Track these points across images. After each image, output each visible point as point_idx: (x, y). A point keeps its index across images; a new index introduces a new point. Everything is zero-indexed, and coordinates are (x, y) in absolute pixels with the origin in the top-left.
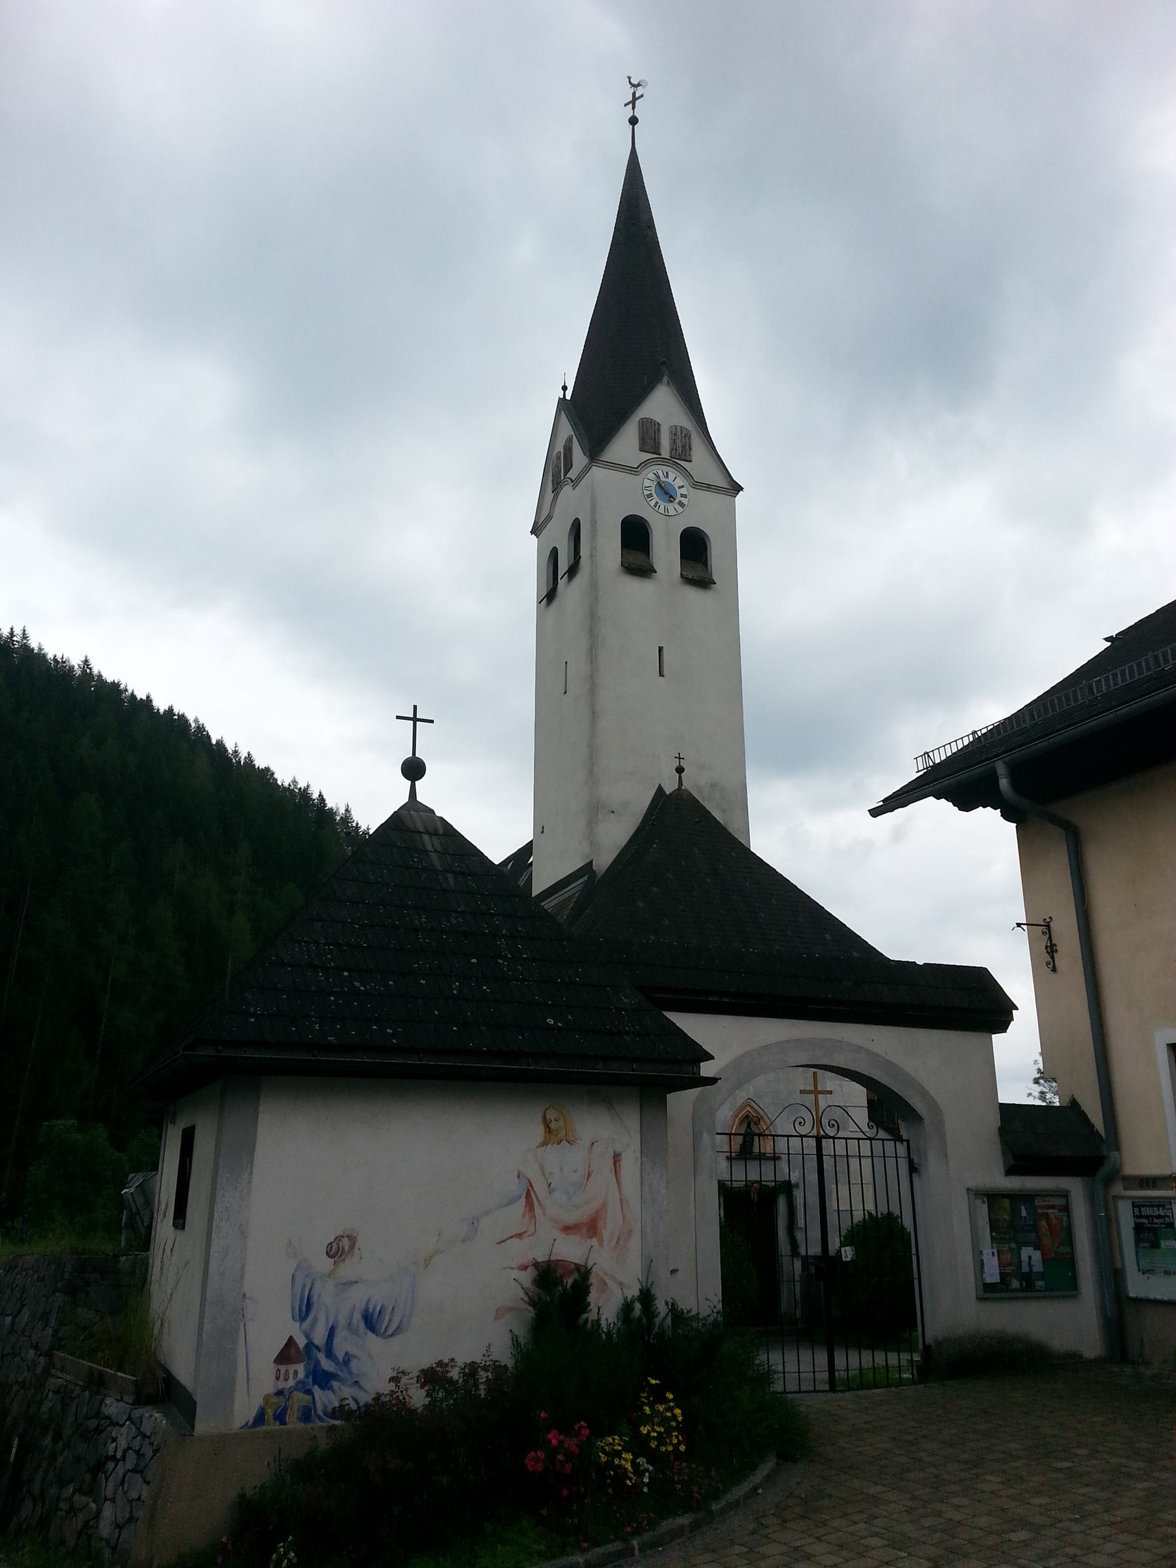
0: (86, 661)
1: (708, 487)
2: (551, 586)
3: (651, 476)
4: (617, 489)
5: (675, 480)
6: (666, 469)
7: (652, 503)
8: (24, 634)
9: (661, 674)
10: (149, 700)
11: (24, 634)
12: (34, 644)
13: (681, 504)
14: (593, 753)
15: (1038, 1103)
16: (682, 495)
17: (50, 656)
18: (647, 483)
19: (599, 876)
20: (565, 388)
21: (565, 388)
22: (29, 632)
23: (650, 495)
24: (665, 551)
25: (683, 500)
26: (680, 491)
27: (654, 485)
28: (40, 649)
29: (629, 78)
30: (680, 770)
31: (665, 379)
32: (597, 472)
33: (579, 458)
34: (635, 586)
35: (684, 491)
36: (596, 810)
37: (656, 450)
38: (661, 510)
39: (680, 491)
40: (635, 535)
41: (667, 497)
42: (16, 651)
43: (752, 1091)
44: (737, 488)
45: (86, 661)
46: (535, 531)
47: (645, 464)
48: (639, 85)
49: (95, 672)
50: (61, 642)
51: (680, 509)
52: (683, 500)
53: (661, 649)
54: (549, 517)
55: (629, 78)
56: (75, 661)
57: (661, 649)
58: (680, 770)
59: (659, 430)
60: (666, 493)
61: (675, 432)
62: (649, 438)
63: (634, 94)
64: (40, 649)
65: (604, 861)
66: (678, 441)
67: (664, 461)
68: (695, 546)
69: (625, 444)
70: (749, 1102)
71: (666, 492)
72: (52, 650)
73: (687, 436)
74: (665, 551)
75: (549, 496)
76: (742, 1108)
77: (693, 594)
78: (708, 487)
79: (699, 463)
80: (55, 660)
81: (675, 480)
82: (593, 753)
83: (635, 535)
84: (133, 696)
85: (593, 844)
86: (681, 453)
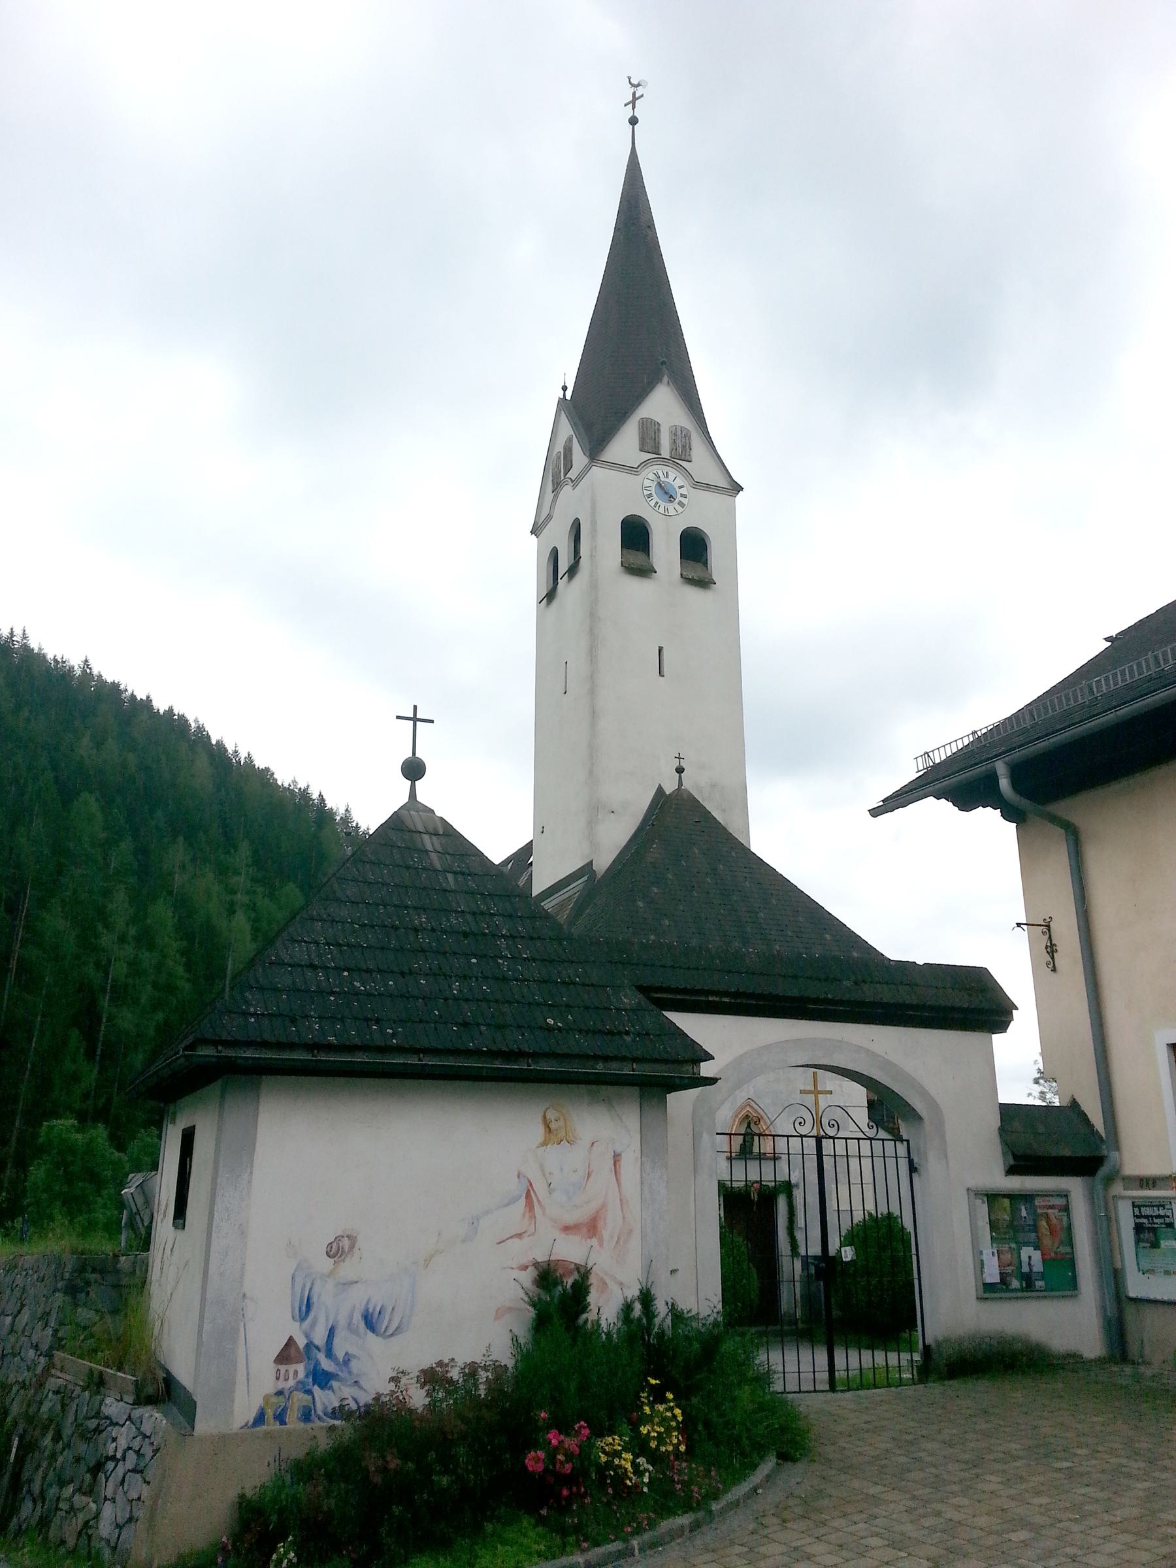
3: (651, 476)
4: (616, 489)
5: (675, 480)
6: (666, 469)
9: (661, 674)
14: (593, 753)
16: (682, 495)
17: (50, 656)
18: (647, 483)
20: (565, 388)
21: (565, 388)
23: (650, 496)
24: (665, 550)
25: (683, 500)
27: (654, 484)
28: (40, 649)
29: (629, 78)
30: (680, 770)
31: (666, 379)
34: (635, 584)
35: (683, 491)
36: (596, 810)
38: (661, 510)
40: (635, 535)
41: (667, 497)
43: (752, 1090)
44: (738, 488)
46: (535, 531)
47: (645, 463)
48: (639, 85)
49: (95, 672)
51: (680, 509)
52: (683, 500)
54: (549, 517)
55: (629, 78)
59: (659, 430)
62: (649, 439)
64: (40, 649)
65: (603, 862)
66: (678, 442)
69: (625, 444)
70: (749, 1101)
73: (687, 436)
74: (665, 550)
75: (549, 496)
76: (742, 1108)
77: (693, 594)
80: (55, 660)
81: (675, 480)
82: (593, 753)
83: (635, 535)
86: (681, 455)
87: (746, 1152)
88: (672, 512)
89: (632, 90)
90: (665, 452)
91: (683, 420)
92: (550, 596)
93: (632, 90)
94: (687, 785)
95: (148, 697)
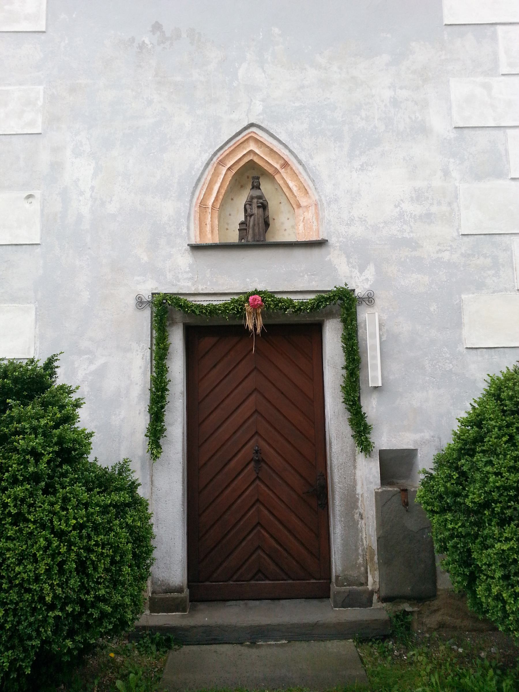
15: (34, 312)
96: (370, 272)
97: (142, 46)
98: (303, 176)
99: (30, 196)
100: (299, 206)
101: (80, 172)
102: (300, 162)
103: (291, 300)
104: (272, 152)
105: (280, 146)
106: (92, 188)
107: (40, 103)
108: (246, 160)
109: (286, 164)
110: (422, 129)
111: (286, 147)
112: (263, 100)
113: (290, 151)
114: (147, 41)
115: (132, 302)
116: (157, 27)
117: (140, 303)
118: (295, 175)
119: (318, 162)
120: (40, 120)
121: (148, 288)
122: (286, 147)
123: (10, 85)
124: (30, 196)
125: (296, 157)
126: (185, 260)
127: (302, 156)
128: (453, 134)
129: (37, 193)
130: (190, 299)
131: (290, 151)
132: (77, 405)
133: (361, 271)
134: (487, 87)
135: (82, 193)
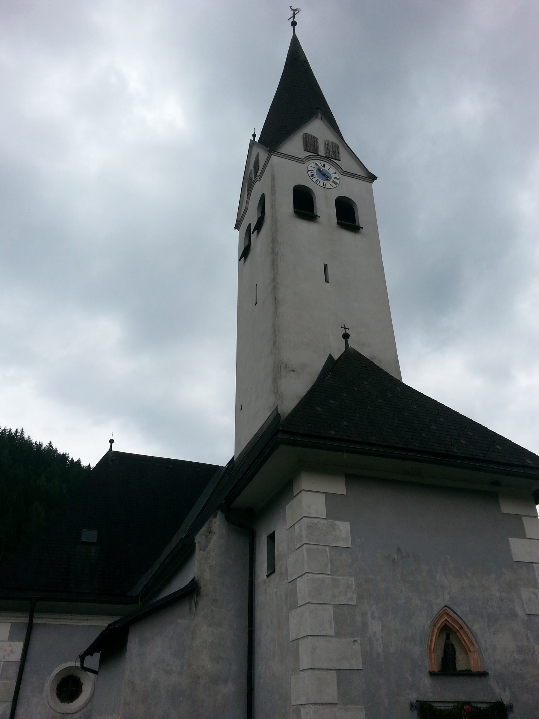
0: (50, 444)
1: (353, 175)
2: (247, 243)
3: (313, 165)
4: (290, 170)
5: (328, 168)
6: (323, 163)
7: (315, 180)
8: (22, 431)
9: (327, 282)
10: (79, 461)
11: (22, 431)
12: (26, 436)
13: (334, 182)
14: (276, 330)
15: (364, 711)
16: (335, 178)
17: (34, 442)
18: (310, 168)
19: (283, 418)
20: (254, 136)
21: (254, 136)
22: (24, 430)
23: (313, 175)
24: (325, 208)
25: (336, 180)
26: (333, 176)
27: (315, 170)
28: (29, 438)
29: (291, 7)
30: (346, 336)
31: (320, 115)
32: (275, 159)
33: (263, 156)
34: (303, 225)
35: (336, 176)
36: (279, 369)
37: (315, 151)
38: (321, 184)
39: (333, 176)
40: (304, 203)
41: (324, 178)
42: (17, 440)
43: (447, 597)
44: (372, 178)
45: (50, 444)
46: (237, 227)
47: (308, 158)
48: (296, 10)
49: (54, 448)
50: (38, 435)
51: (334, 186)
52: (336, 180)
53: (325, 266)
54: (246, 210)
55: (291, 7)
56: (45, 444)
57: (325, 266)
58: (346, 336)
59: (317, 141)
60: (324, 175)
61: (327, 144)
62: (310, 144)
63: (294, 13)
64: (29, 438)
65: (288, 406)
66: (330, 149)
67: (321, 158)
68: (347, 214)
69: (294, 145)
70: (446, 610)
71: (326, 176)
72: (35, 439)
73: (336, 146)
74: (325, 208)
75: (246, 197)
76: (440, 616)
77: (347, 236)
78: (353, 175)
79: (345, 161)
80: (36, 443)
81: (328, 168)
82: (276, 330)
83: (304, 203)
84: (72, 460)
85: (277, 392)
86: (332, 156)
87: (448, 667)
88: (328, 186)
89: (293, 11)
90: (322, 151)
91: (332, 138)
92: (245, 254)
93: (293, 11)
94: (351, 345)
95: (79, 460)
96: (507, 693)
97: (394, 560)
98: (470, 635)
99: (355, 641)
100: (470, 651)
101: (375, 627)
102: (468, 627)
103: (480, 708)
104: (454, 620)
105: (458, 618)
106: (382, 638)
107: (354, 587)
108: (443, 624)
109: (461, 627)
110: (513, 614)
111: (461, 619)
112: (448, 594)
113: (463, 621)
114: (396, 558)
115: (407, 706)
116: (399, 550)
117: (412, 707)
118: (465, 633)
119: (476, 628)
120: (355, 597)
121: (414, 697)
122: (461, 619)
123: (338, 575)
124: (355, 641)
125: (466, 625)
126: (427, 681)
127: (469, 625)
128: (526, 618)
129: (358, 639)
130: (435, 705)
131: (463, 621)
132: (22, 432)
133: (504, 691)
134: (535, 594)
135: (378, 640)
